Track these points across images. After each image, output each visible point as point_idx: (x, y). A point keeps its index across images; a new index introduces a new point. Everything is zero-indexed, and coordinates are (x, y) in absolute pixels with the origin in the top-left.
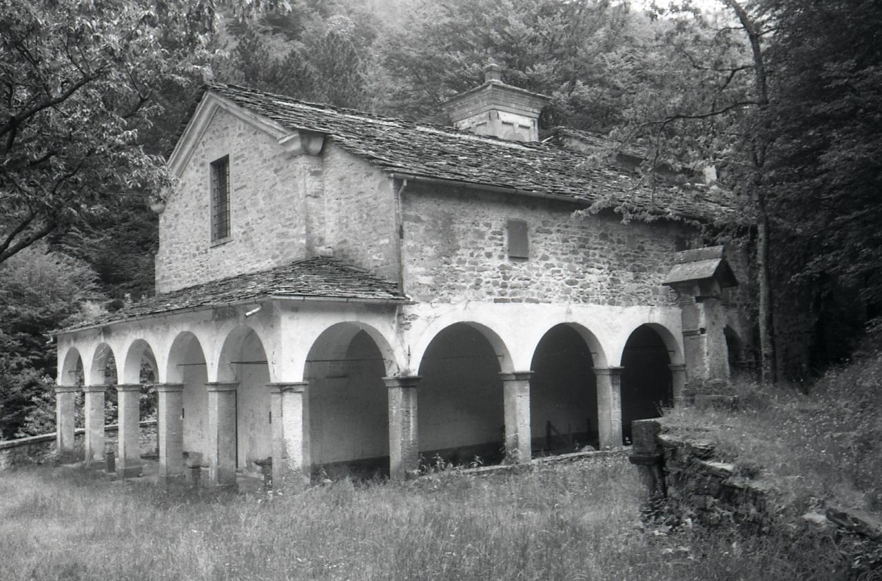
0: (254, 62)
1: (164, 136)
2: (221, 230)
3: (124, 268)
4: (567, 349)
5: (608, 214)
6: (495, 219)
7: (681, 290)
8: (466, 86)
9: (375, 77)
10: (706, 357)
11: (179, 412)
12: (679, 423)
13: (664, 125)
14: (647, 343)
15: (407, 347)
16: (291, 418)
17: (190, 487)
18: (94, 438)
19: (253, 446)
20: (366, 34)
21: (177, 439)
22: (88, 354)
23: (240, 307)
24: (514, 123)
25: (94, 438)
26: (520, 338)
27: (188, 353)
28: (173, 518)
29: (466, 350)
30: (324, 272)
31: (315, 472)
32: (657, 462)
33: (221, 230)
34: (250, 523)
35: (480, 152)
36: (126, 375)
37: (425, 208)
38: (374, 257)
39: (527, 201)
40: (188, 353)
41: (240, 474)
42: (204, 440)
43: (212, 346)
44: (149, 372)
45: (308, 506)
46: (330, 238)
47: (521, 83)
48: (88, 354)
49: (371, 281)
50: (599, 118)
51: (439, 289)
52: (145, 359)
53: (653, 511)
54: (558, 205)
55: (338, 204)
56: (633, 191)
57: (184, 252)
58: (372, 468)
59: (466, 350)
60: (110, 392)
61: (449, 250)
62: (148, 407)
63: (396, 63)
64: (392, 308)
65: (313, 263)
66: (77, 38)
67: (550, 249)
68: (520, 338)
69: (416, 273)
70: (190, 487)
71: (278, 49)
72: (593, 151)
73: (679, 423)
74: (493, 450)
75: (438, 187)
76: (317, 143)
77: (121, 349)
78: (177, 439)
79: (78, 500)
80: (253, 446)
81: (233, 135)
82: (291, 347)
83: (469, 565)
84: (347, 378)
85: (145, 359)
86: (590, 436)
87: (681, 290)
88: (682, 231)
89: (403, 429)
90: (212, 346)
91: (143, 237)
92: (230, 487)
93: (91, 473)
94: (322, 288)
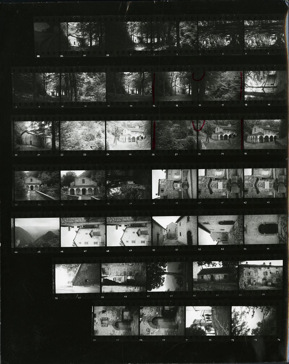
0: (226, 315)
1: (252, 127)
2: (255, 131)
3: (251, 133)
4: (271, 137)
5: (273, 130)
6: (268, 131)
7: (277, 134)
8: (267, 125)
9: (262, 124)
10: (278, 137)
11: (253, 140)
12: (277, 140)
13: (276, 126)
14: (275, 136)
15: (264, 137)
16: (258, 140)
17: (254, 143)
18: (249, 141)
19: (257, 141)
20: (262, 122)
21: (253, 141)
22: (249, 137)
23: (256, 135)
24: (269, 126)
25: (249, 141)
26: (269, 136)
27: (254, 137)
28: (253, 145)
29: (267, 137)
30: (260, 133)
31: (260, 142)
32: (276, 142)
33: (255, 131)
34: (257, 145)
35: (267, 128)
36: (251, 138)
37: (265, 130)
38: (262, 132)
39: (269, 130)
40: (254, 137)
41: (239, 194)
42: (254, 141)
43: (255, 137)
44: (252, 138)
45: (259, 144)
46: (260, 132)
47: (269, 124)
48: (249, 137)
49: (262, 134)
50: (273, 126)
51: (266, 134)
52: (251, 137)
53: (276, 144)
54: (271, 130)
55: (261, 130)
56: (275, 129)
57: (253, 132)
58: (262, 142)
59: (267, 137)
60: (250, 139)
61: (266, 132)
62: (252, 139)
63: (263, 124)
64: (263, 135)
65: (259, 133)
66: (248, 122)
67: (271, 133)
68: (269, 136)
69: (264, 133)
70: (254, 143)
71: (258, 123)
72: (273, 127)
73: (277, 140)
74: (268, 141)
75: (265, 129)
76: (260, 127)
77: (250, 137)
78: (253, 141)
79: (248, 144)
80: (257, 141)
81: (256, 127)
82: (258, 137)
83: (65, 280)
84: (261, 138)
85: (251, 137)
86: (273, 141)
87: (277, 134)
88: (277, 131)
89: (264, 141)
90: (255, 137)
91: (251, 131)
92: (256, 143)
93: (249, 143)
94: (260, 134)
